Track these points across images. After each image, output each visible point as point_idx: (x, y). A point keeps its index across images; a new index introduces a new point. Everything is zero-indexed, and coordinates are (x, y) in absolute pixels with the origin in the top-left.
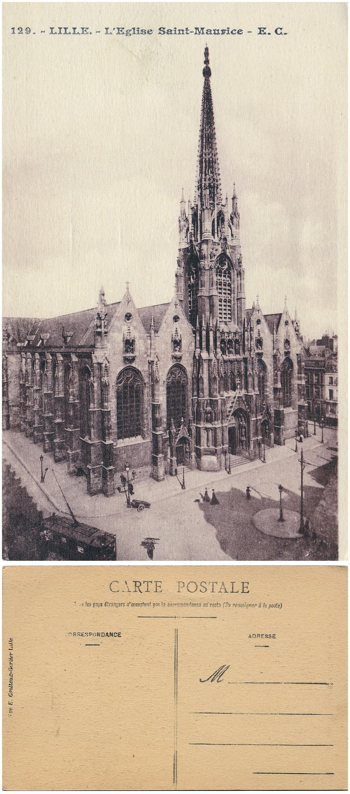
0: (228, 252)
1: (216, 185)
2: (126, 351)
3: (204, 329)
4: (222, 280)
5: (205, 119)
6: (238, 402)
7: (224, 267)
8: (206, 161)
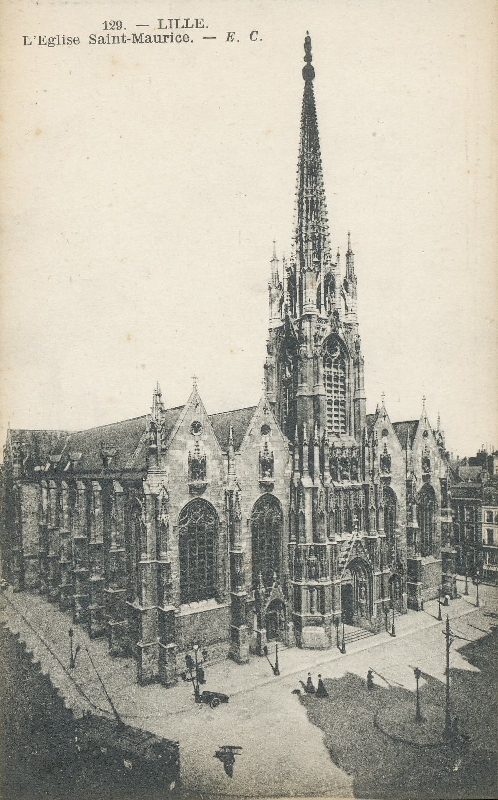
0: (341, 332)
1: (322, 236)
2: (193, 477)
3: (305, 444)
4: (332, 373)
5: (306, 141)
7: (334, 355)
8: (307, 202)
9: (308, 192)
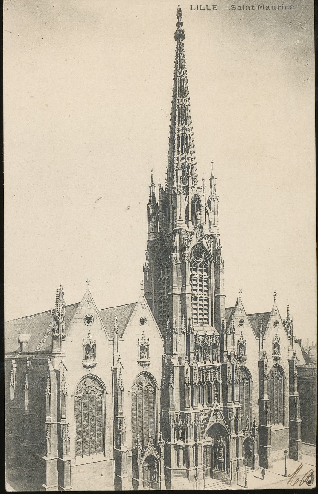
6: (215, 416)
8: (178, 138)
9: (179, 130)
